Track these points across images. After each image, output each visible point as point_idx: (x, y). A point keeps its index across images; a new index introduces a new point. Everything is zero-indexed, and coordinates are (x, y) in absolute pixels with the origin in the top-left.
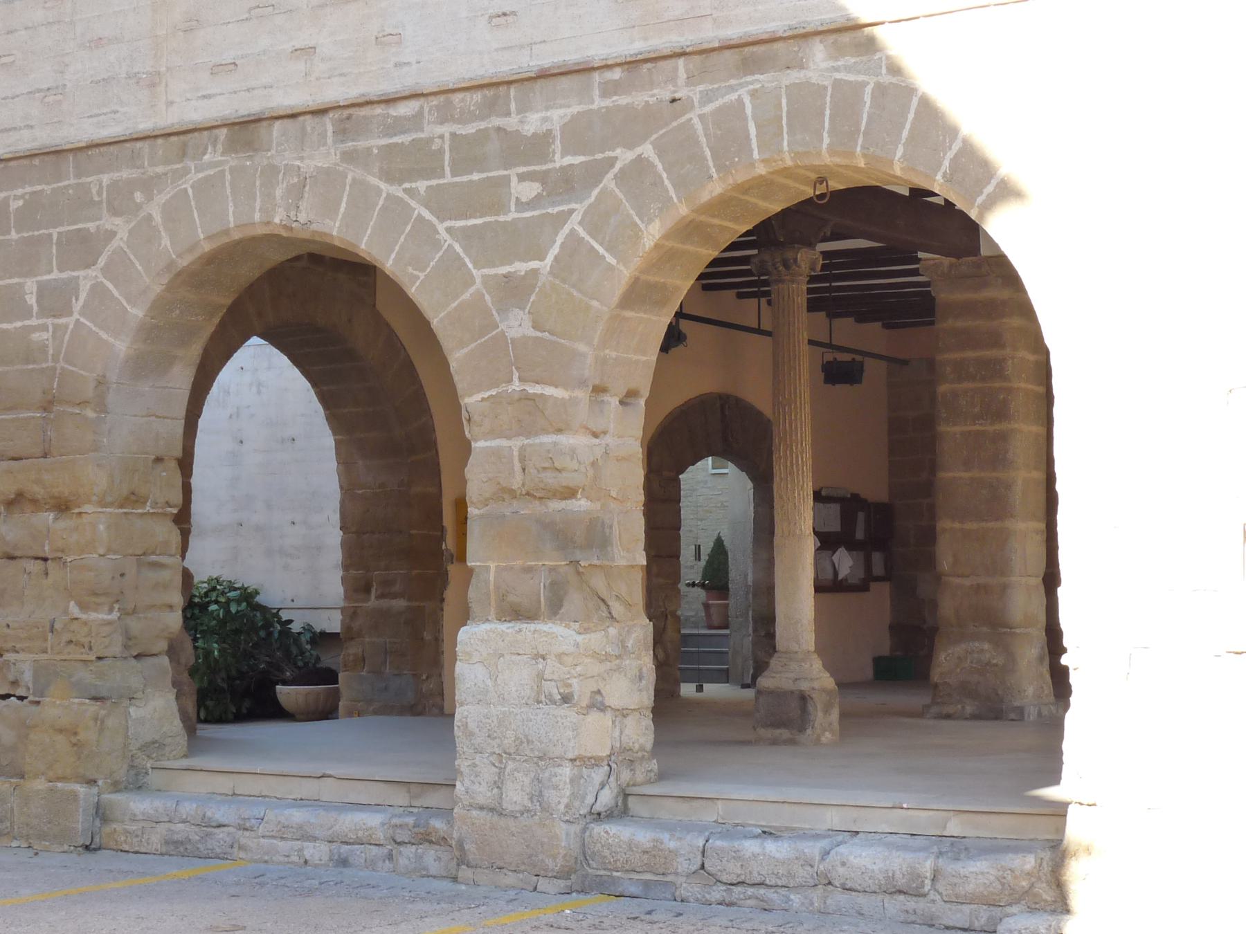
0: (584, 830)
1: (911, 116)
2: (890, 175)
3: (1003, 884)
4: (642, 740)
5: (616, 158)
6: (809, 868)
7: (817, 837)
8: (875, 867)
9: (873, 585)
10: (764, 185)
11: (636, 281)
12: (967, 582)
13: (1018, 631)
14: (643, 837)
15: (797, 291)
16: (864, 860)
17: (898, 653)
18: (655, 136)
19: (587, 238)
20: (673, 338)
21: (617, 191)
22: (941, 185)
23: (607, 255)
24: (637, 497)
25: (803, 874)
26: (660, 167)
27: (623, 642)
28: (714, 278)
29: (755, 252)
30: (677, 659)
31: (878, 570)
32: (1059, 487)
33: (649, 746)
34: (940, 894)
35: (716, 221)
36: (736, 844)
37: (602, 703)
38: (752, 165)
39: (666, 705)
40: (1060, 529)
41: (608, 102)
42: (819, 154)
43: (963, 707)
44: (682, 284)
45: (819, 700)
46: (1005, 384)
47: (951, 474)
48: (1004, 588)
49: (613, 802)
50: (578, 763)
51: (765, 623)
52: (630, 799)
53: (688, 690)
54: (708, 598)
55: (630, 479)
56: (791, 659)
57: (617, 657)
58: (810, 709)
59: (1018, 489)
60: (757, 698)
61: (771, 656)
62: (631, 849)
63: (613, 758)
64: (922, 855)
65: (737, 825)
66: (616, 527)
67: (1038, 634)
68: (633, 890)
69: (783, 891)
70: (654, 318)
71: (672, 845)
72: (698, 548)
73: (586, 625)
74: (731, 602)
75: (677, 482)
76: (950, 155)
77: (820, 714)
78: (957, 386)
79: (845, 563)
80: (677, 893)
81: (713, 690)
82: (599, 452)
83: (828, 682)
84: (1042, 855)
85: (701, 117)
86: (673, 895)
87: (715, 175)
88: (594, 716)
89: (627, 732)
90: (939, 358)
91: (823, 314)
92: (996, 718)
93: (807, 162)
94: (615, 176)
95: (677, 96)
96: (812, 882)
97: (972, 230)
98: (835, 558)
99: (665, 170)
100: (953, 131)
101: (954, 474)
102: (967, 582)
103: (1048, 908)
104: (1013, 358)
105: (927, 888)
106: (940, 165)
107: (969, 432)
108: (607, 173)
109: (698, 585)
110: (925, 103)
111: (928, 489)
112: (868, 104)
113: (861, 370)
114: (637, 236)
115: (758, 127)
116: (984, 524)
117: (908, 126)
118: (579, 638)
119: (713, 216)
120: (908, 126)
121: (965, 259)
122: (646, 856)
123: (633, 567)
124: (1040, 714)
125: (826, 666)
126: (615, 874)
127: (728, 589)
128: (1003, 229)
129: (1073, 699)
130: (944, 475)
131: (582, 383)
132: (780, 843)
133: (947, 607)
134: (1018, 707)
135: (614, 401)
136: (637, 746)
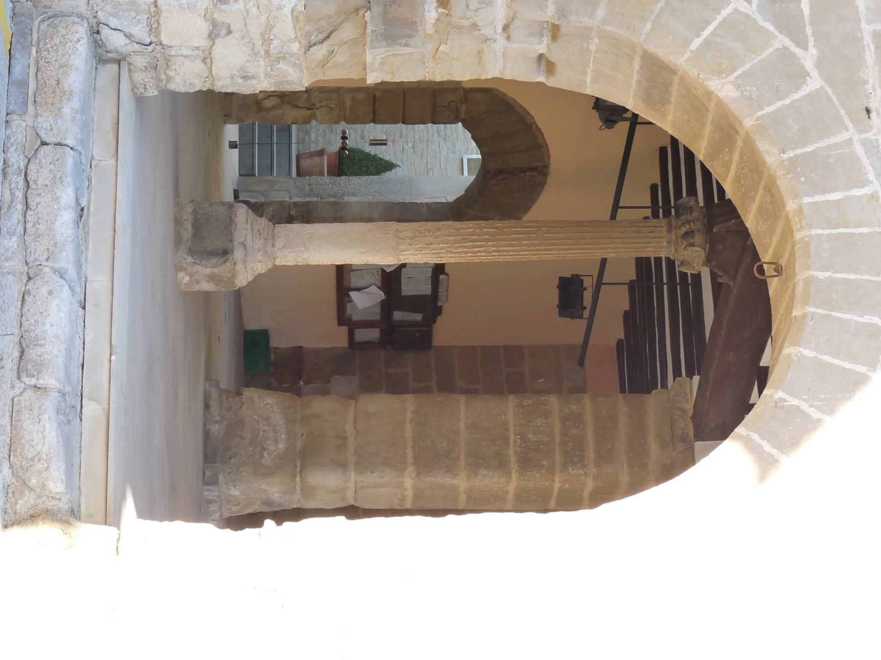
0: (81, 16)
1: (846, 365)
2: (784, 340)
3: (32, 459)
4: (178, 79)
5: (806, 49)
6: (45, 256)
7: (79, 265)
8: (48, 325)
9: (344, 329)
10: (774, 207)
11: (672, 71)
12: (349, 427)
13: (298, 479)
14: (75, 80)
15: (659, 244)
16: (55, 314)
17: (272, 356)
18: (829, 90)
19: (720, 18)
20: (609, 113)
21: (771, 50)
22: (771, 396)
23: (701, 39)
24: (439, 74)
25: (39, 250)
26: (796, 97)
27: (284, 58)
28: (675, 157)
29: (702, 204)
30: (262, 118)
31: (362, 335)
32: (451, 517)
33: (172, 87)
34: (21, 394)
35: (736, 157)
36: (69, 179)
37: (217, 36)
38: (796, 196)
39: (217, 106)
40: (406, 519)
41: (868, 39)
42: (807, 267)
44: (668, 122)
45: (223, 270)
46: (558, 467)
47: (462, 408)
48: (343, 465)
49: (112, 48)
50: (153, 9)
51: (305, 214)
52: (115, 67)
53: (232, 132)
54: (329, 155)
55: (457, 64)
56: (266, 240)
57: (267, 53)
58: (214, 260)
59: (447, 480)
60: (223, 204)
61: (270, 220)
62: (61, 66)
63: (159, 48)
64: (62, 375)
65: (90, 181)
66: (407, 50)
67: (295, 501)
68: (17, 69)
69: (20, 229)
70: (632, 90)
71: (67, 111)
72: (383, 143)
73: (301, 18)
74: (326, 179)
75: (455, 121)
76: (804, 406)
77: (208, 271)
79: (366, 301)
80: (15, 117)
81: (232, 159)
82: (487, 32)
83: (242, 280)
84: (65, 500)
85: (850, 141)
86: (13, 112)
87: (785, 156)
88: (204, 27)
89: (188, 63)
90: (587, 398)
91: (634, 277)
92: (206, 457)
93: (798, 254)
94: (786, 49)
95: (873, 115)
96: (30, 259)
97: (722, 432)
98: (374, 289)
99: (793, 102)
100: (830, 410)
101: (463, 413)
102: (349, 427)
103: (8, 506)
104: (586, 475)
105: (26, 380)
106: (793, 395)
107: (507, 429)
108: (791, 39)
109: (344, 143)
110: (858, 381)
111: (447, 387)
112: (860, 319)
114: (720, 72)
115: (837, 202)
116: (410, 443)
117: (836, 362)
118: (287, 11)
119: (742, 155)
120: (836, 362)
122: (54, 83)
123: (365, 69)
124: (210, 502)
125: (258, 277)
126: (34, 50)
127: (340, 175)
128: (725, 462)
129: (228, 531)
131: (562, 13)
132: (71, 226)
133: (322, 406)
135: (542, 49)
136: (171, 74)
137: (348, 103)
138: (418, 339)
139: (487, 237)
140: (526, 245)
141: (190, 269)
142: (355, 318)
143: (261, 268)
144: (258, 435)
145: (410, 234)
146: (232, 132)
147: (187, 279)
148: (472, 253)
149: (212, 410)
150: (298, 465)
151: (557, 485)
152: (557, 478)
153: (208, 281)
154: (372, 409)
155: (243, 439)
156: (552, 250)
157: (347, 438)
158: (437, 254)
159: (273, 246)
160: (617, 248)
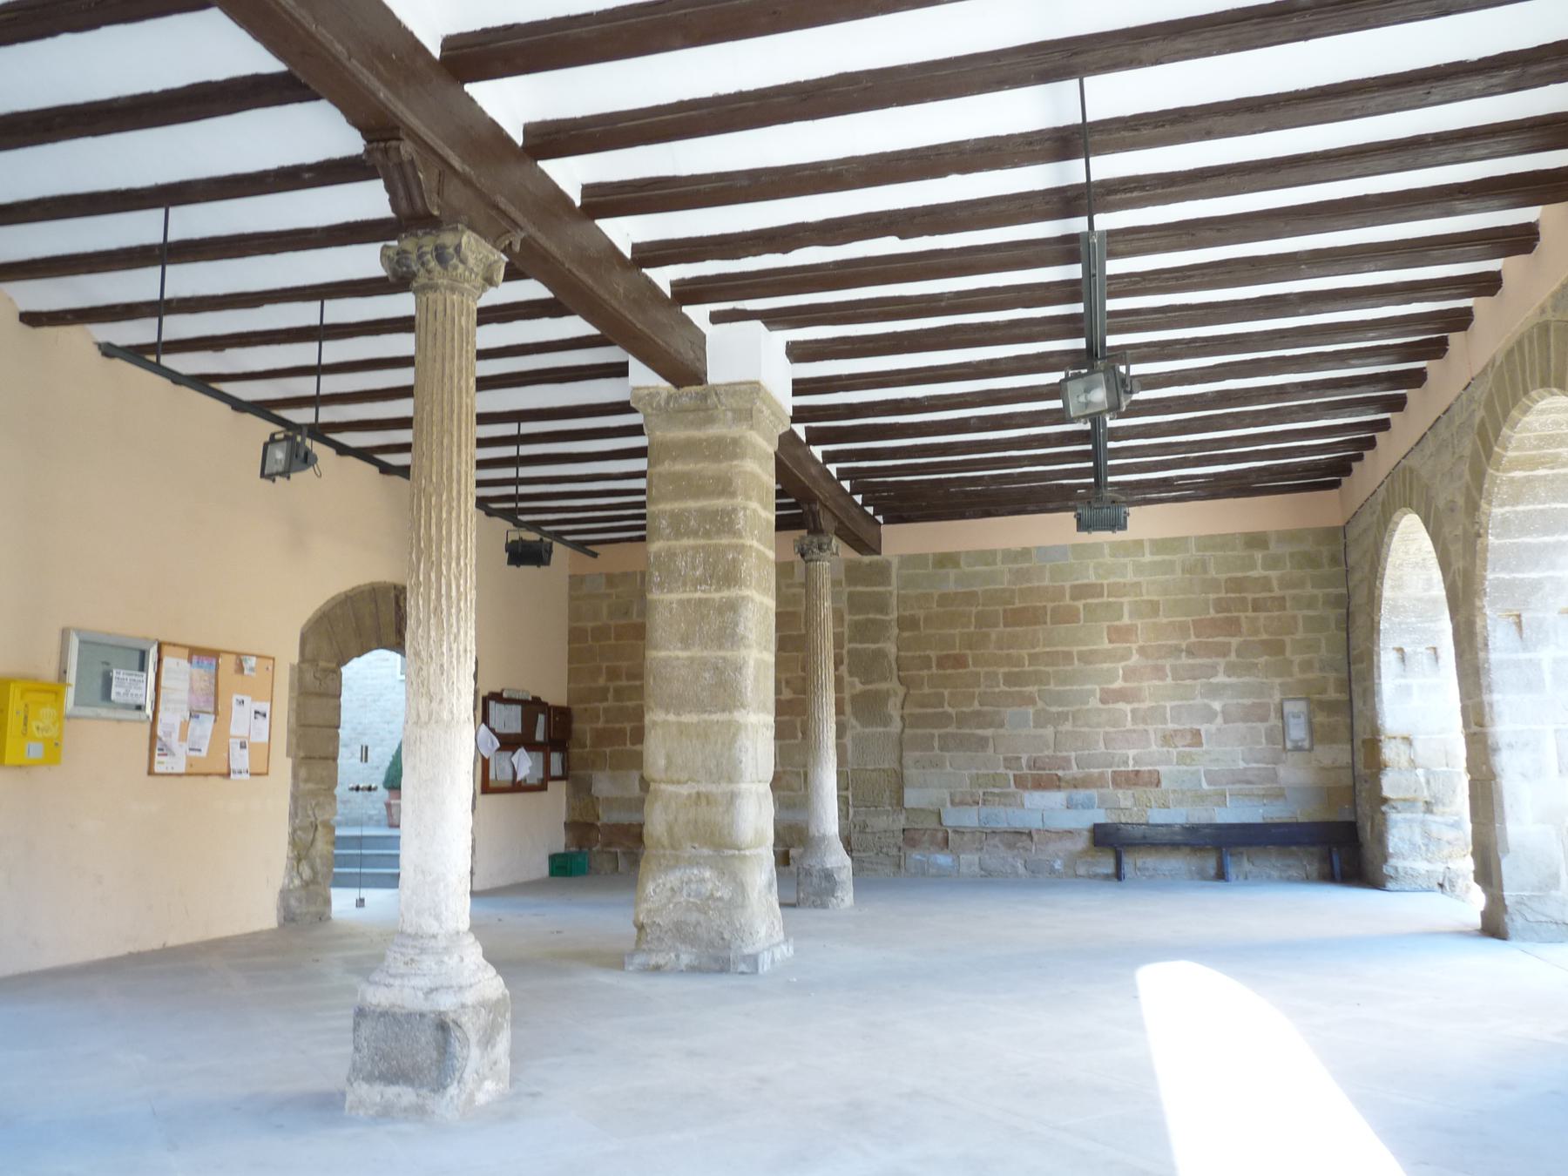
9: (551, 785)
12: (684, 790)
13: (747, 853)
17: (573, 849)
31: (556, 769)
43: (677, 956)
45: (472, 1026)
46: (735, 541)
47: (663, 654)
48: (732, 797)
56: (423, 951)
58: (456, 1047)
59: (750, 671)
78: (673, 543)
79: (525, 764)
83: (491, 985)
101: (669, 653)
102: (684, 790)
104: (745, 509)
107: (689, 601)
113: (550, 552)
116: (706, 716)
121: (686, 389)
130: (656, 655)
134: (749, 956)
137: (310, 786)
138: (561, 720)
139: (433, 576)
140: (449, 513)
141: (470, 1086)
142: (541, 775)
143: (473, 953)
144: (694, 904)
145: (424, 701)
146: (342, 901)
147: (489, 1085)
148: (459, 601)
149: (662, 962)
150: (731, 852)
151: (755, 543)
152: (748, 542)
153: (493, 1046)
154: (662, 762)
155: (698, 923)
156: (459, 472)
157: (698, 794)
158: (459, 657)
159: (434, 937)
160: (460, 371)
